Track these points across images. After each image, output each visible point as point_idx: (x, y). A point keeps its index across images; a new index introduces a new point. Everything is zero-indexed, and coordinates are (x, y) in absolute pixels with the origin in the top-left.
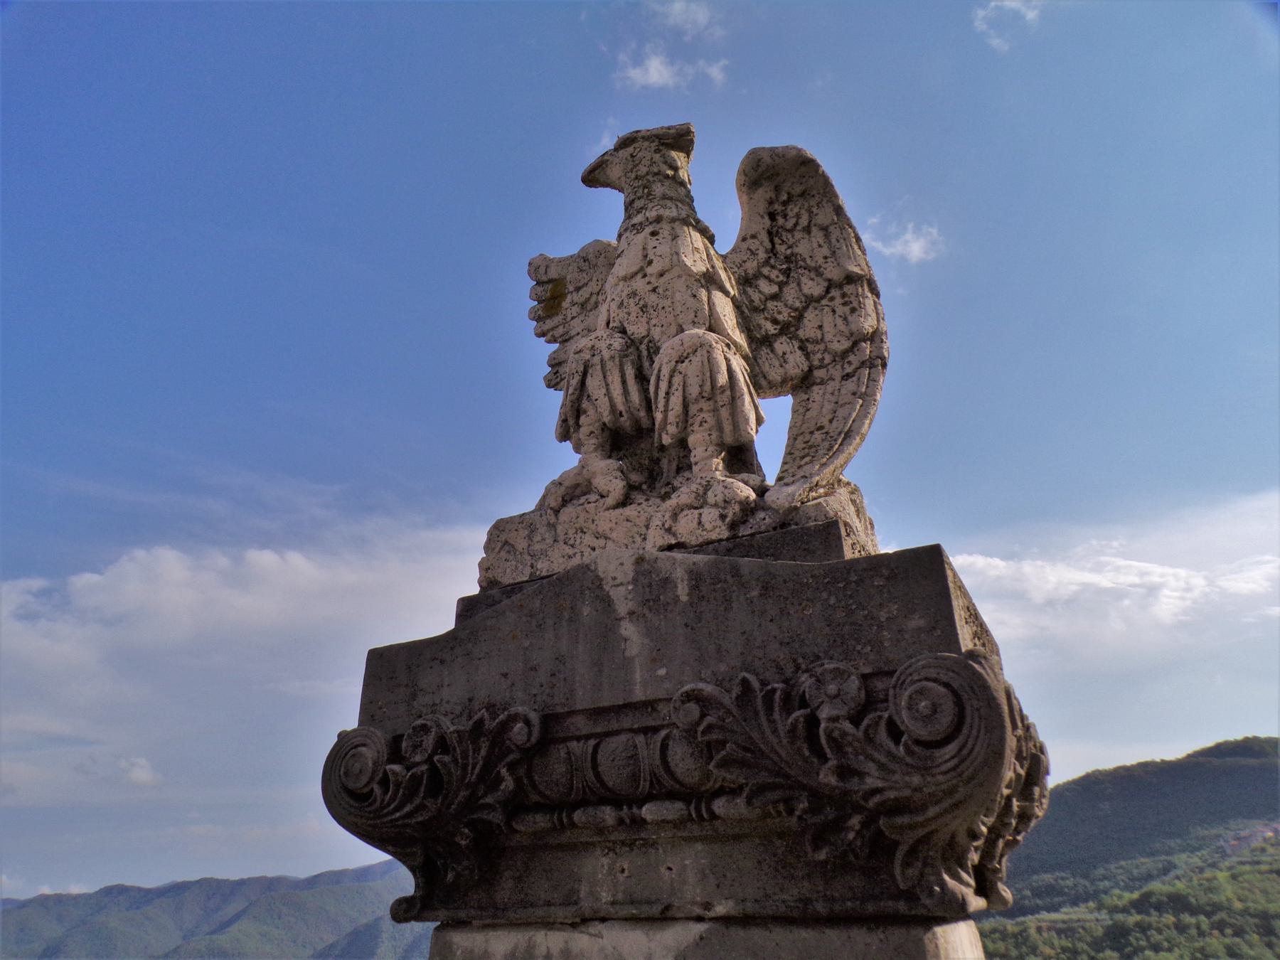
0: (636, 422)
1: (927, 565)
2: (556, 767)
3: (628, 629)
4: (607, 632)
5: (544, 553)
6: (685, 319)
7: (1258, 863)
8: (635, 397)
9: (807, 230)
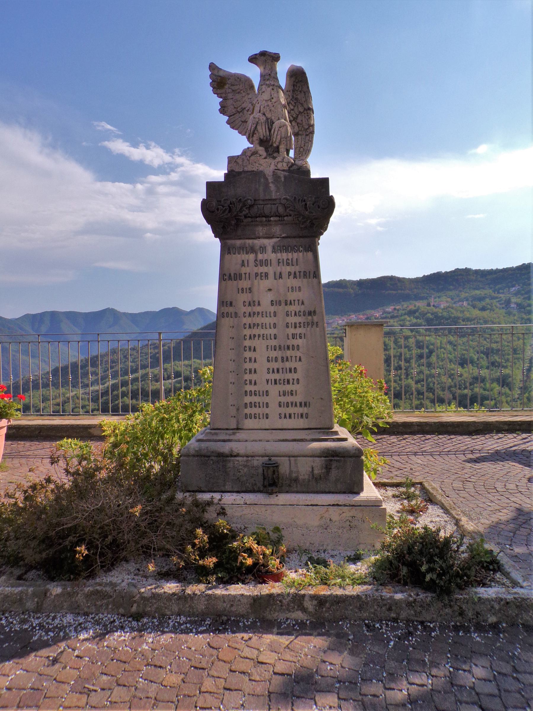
0: (267, 138)
1: (324, 183)
2: (255, 210)
3: (271, 185)
4: (267, 186)
5: (246, 166)
6: (280, 116)
7: (333, 334)
8: (268, 133)
9: (301, 92)
